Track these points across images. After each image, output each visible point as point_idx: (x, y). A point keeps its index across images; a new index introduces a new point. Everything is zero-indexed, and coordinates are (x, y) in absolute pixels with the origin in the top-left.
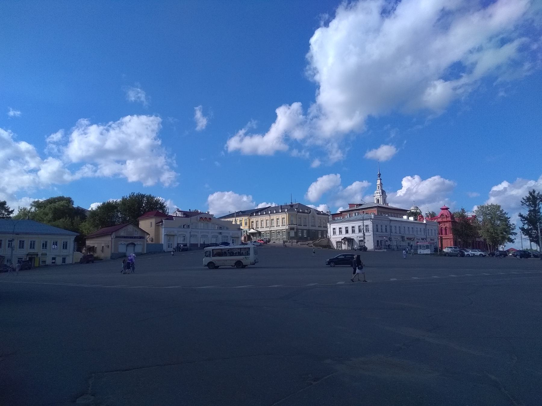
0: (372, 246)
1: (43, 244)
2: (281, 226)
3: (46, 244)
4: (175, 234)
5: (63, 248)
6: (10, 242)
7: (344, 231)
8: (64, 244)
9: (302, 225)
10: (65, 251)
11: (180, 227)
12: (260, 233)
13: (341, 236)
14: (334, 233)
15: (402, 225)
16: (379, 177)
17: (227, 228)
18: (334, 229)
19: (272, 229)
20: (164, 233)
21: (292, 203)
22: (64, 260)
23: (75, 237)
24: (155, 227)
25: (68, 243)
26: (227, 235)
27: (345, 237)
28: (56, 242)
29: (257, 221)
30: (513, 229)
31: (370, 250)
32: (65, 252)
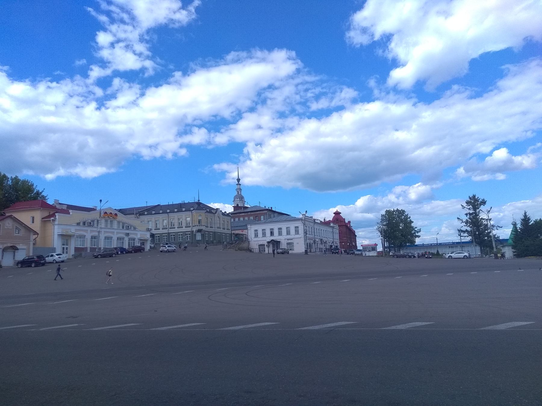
0: (303, 249)
7: (268, 233)
9: (161, 229)
11: (78, 224)
13: (264, 238)
14: (256, 235)
18: (256, 231)
19: (171, 231)
27: (272, 240)
30: (418, 232)
31: (300, 253)
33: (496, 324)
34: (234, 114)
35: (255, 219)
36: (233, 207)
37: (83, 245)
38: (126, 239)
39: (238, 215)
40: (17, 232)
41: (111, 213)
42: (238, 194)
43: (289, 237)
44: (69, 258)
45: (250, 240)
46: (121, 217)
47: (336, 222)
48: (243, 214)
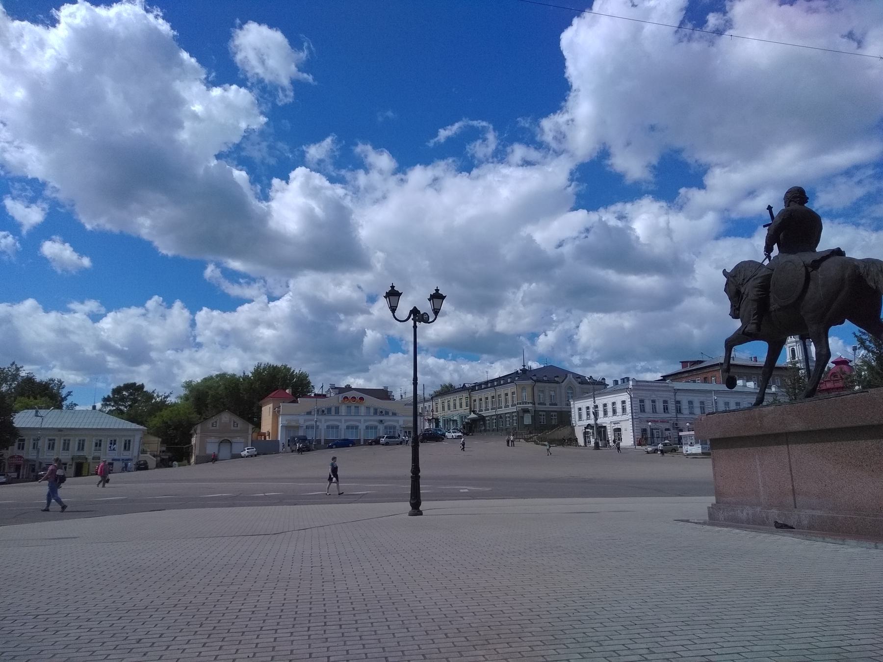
2: (503, 407)
10: (126, 453)
17: (394, 414)
18: (580, 409)
19: (500, 412)
21: (524, 366)
25: (132, 441)
28: (115, 441)
29: (506, 395)
34: (229, 160)
38: (381, 427)
39: (679, 376)
41: (354, 398)
43: (615, 418)
44: (727, 436)
45: (574, 425)
46: (370, 400)
47: (834, 381)
48: (687, 375)
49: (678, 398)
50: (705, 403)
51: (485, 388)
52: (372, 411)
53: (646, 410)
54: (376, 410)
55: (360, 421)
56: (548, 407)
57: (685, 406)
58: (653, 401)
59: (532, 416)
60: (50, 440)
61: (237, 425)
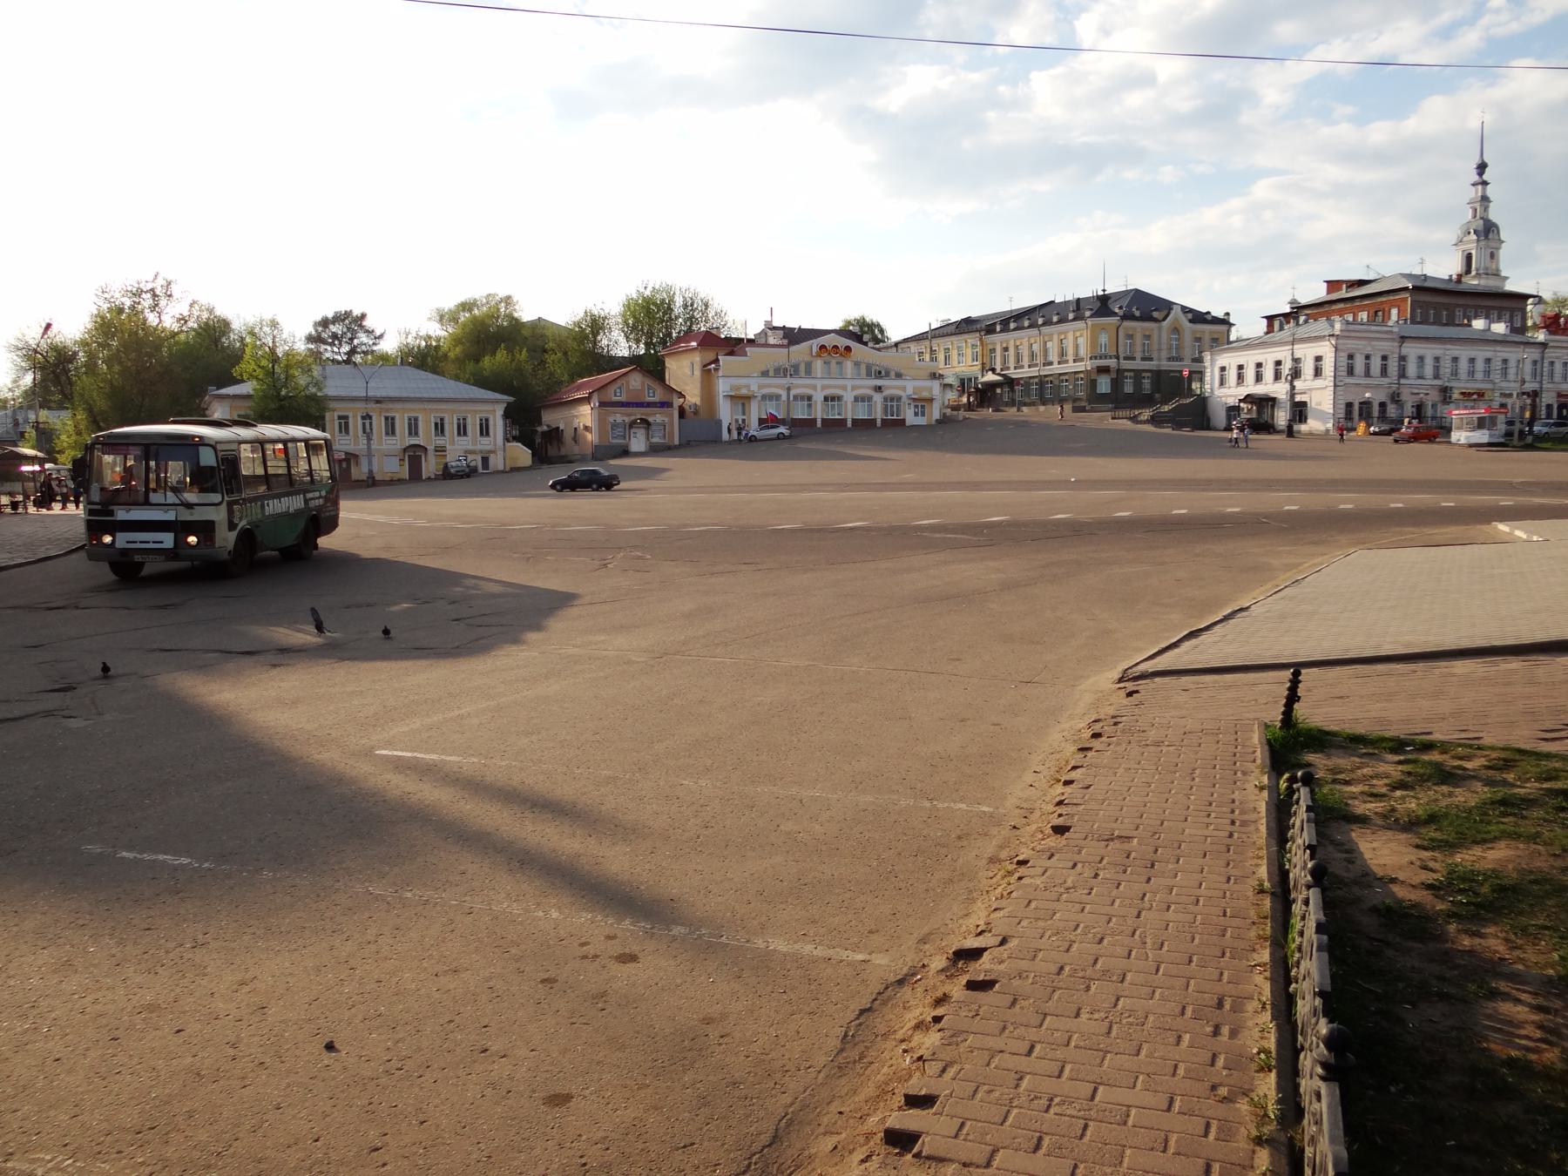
1: (436, 424)
3: (442, 425)
4: (750, 393)
5: (482, 434)
6: (343, 421)
7: (1250, 374)
8: (481, 425)
10: (485, 440)
11: (765, 374)
12: (1010, 382)
15: (1447, 352)
16: (1481, 174)
19: (1046, 371)
20: (724, 392)
22: (485, 460)
23: (505, 405)
24: (702, 375)
26: (899, 392)
27: (1248, 395)
32: (485, 444)
33: (847, 523)
35: (1373, 318)
36: (1325, 284)
37: (810, 414)
39: (1326, 308)
40: (651, 395)
41: (836, 347)
42: (1475, 217)
48: (1341, 306)
49: (1404, 351)
50: (1441, 360)
51: (1014, 330)
52: (863, 371)
53: (1372, 373)
54: (869, 368)
55: (844, 388)
56: (1138, 364)
57: (1412, 369)
58: (1368, 357)
59: (1112, 379)
60: (340, 418)
61: (654, 392)
